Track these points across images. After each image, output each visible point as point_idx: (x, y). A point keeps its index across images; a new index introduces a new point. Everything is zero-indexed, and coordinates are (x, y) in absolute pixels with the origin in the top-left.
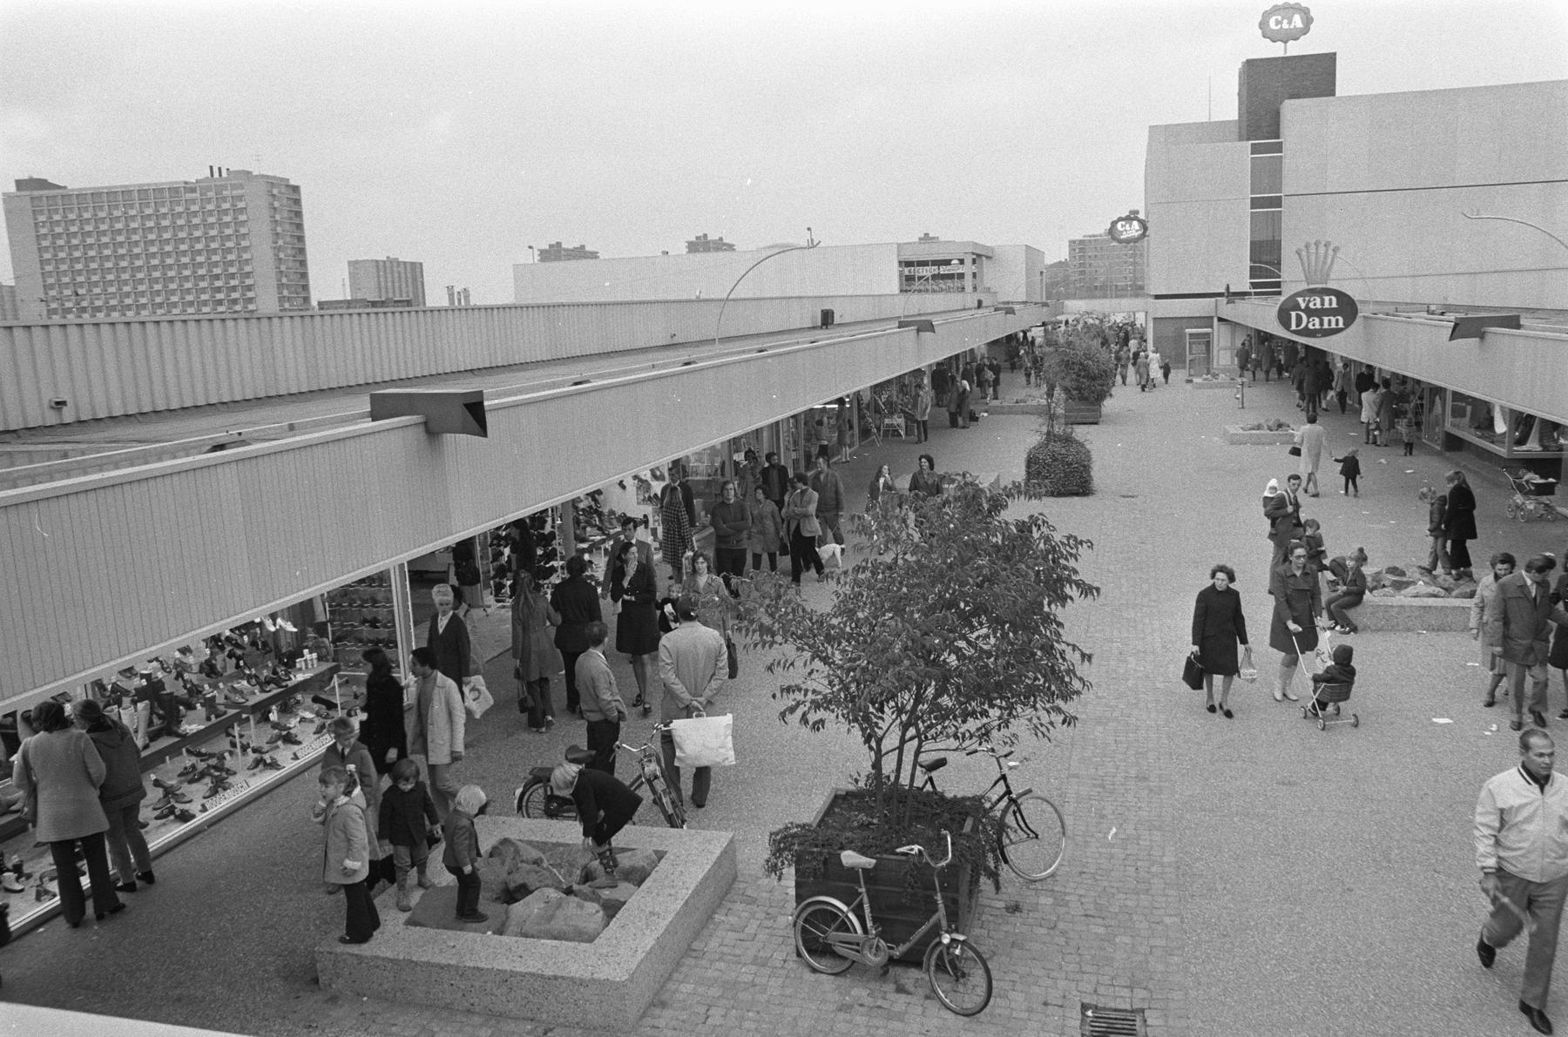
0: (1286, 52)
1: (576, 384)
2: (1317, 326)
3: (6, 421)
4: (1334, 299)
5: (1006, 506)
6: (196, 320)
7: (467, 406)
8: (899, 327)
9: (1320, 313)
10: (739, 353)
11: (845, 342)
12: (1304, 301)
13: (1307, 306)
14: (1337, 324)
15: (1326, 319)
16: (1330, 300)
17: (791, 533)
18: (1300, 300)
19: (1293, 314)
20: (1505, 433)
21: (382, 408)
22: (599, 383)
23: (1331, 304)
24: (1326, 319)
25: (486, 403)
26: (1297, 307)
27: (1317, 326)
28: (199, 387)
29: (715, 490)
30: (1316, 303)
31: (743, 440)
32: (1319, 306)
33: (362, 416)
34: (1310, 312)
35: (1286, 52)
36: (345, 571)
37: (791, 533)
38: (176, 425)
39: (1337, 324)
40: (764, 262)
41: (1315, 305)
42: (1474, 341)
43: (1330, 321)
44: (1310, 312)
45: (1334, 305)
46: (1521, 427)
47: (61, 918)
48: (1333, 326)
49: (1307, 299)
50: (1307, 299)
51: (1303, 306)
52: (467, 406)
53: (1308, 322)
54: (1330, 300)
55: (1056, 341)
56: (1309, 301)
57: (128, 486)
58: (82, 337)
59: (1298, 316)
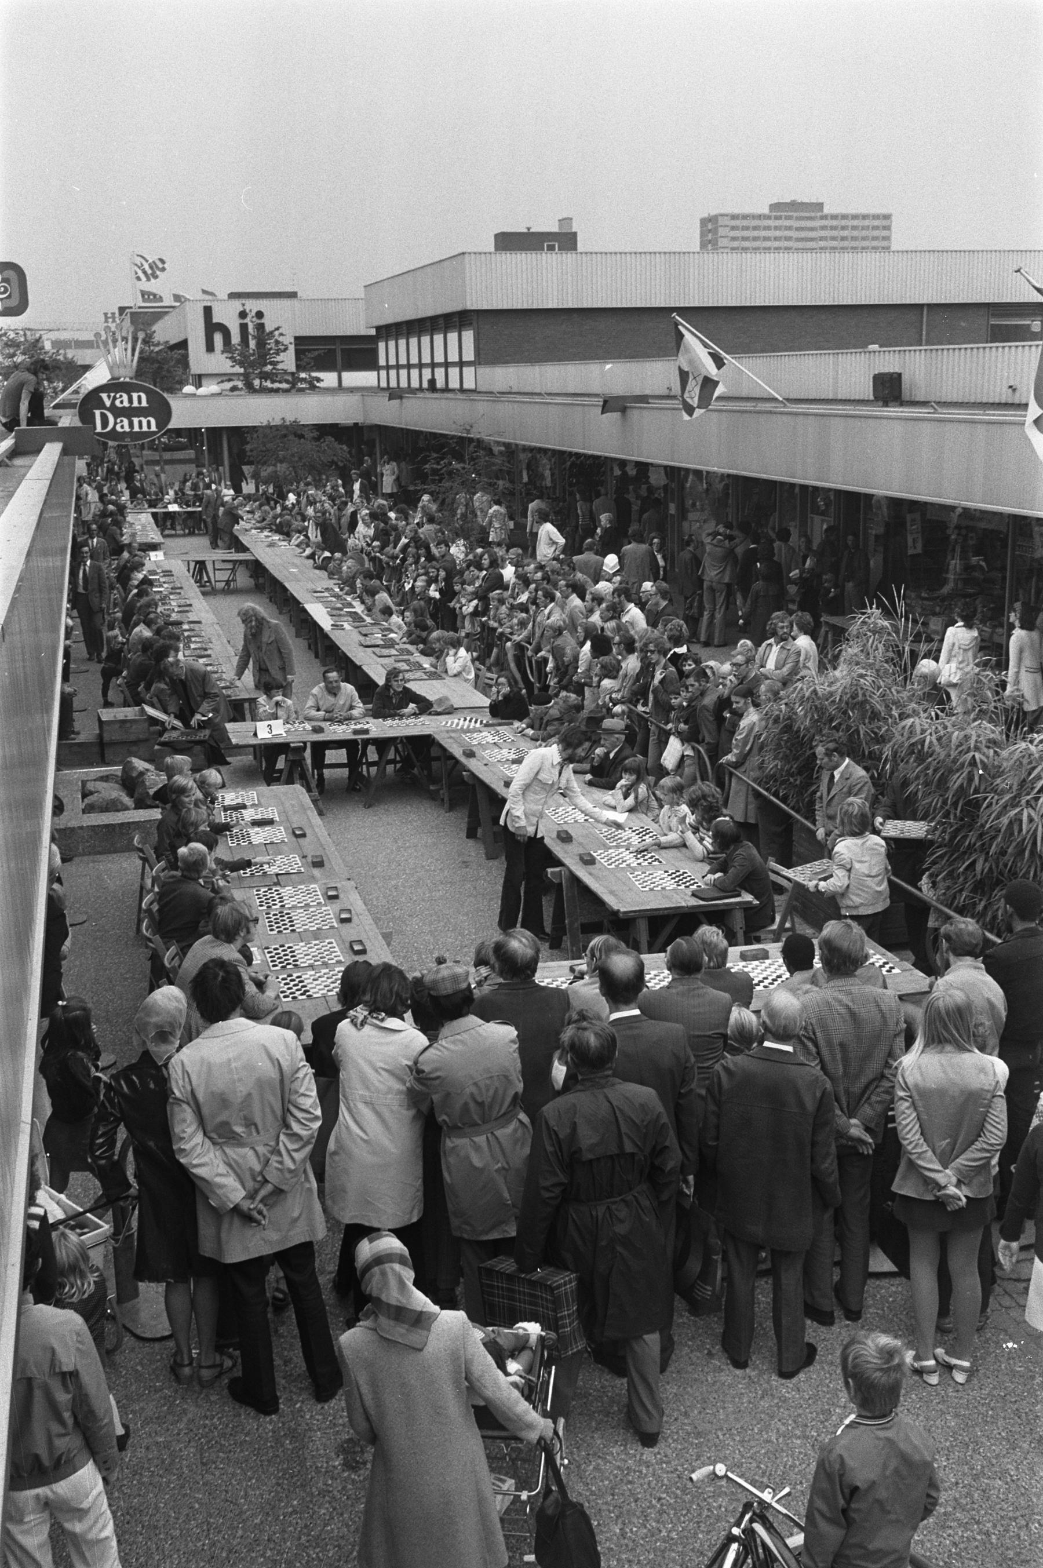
2: (127, 429)
4: (143, 396)
5: (330, 578)
9: (129, 413)
12: (109, 397)
13: (113, 403)
14: (149, 426)
15: (136, 420)
16: (139, 397)
18: (104, 396)
19: (97, 413)
20: (924, 657)
23: (140, 402)
24: (136, 420)
26: (101, 405)
27: (127, 429)
29: (993, 772)
30: (123, 401)
31: (275, 1273)
32: (126, 404)
34: (118, 412)
38: (878, 1283)
39: (149, 426)
41: (122, 402)
42: (398, 401)
43: (140, 422)
44: (118, 412)
45: (144, 404)
46: (471, 782)
47: (463, 333)
48: (145, 428)
49: (112, 395)
50: (112, 395)
51: (108, 403)
53: (116, 424)
54: (139, 397)
56: (115, 398)
59: (103, 416)
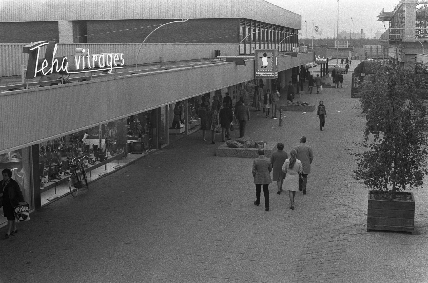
8: (226, 62)
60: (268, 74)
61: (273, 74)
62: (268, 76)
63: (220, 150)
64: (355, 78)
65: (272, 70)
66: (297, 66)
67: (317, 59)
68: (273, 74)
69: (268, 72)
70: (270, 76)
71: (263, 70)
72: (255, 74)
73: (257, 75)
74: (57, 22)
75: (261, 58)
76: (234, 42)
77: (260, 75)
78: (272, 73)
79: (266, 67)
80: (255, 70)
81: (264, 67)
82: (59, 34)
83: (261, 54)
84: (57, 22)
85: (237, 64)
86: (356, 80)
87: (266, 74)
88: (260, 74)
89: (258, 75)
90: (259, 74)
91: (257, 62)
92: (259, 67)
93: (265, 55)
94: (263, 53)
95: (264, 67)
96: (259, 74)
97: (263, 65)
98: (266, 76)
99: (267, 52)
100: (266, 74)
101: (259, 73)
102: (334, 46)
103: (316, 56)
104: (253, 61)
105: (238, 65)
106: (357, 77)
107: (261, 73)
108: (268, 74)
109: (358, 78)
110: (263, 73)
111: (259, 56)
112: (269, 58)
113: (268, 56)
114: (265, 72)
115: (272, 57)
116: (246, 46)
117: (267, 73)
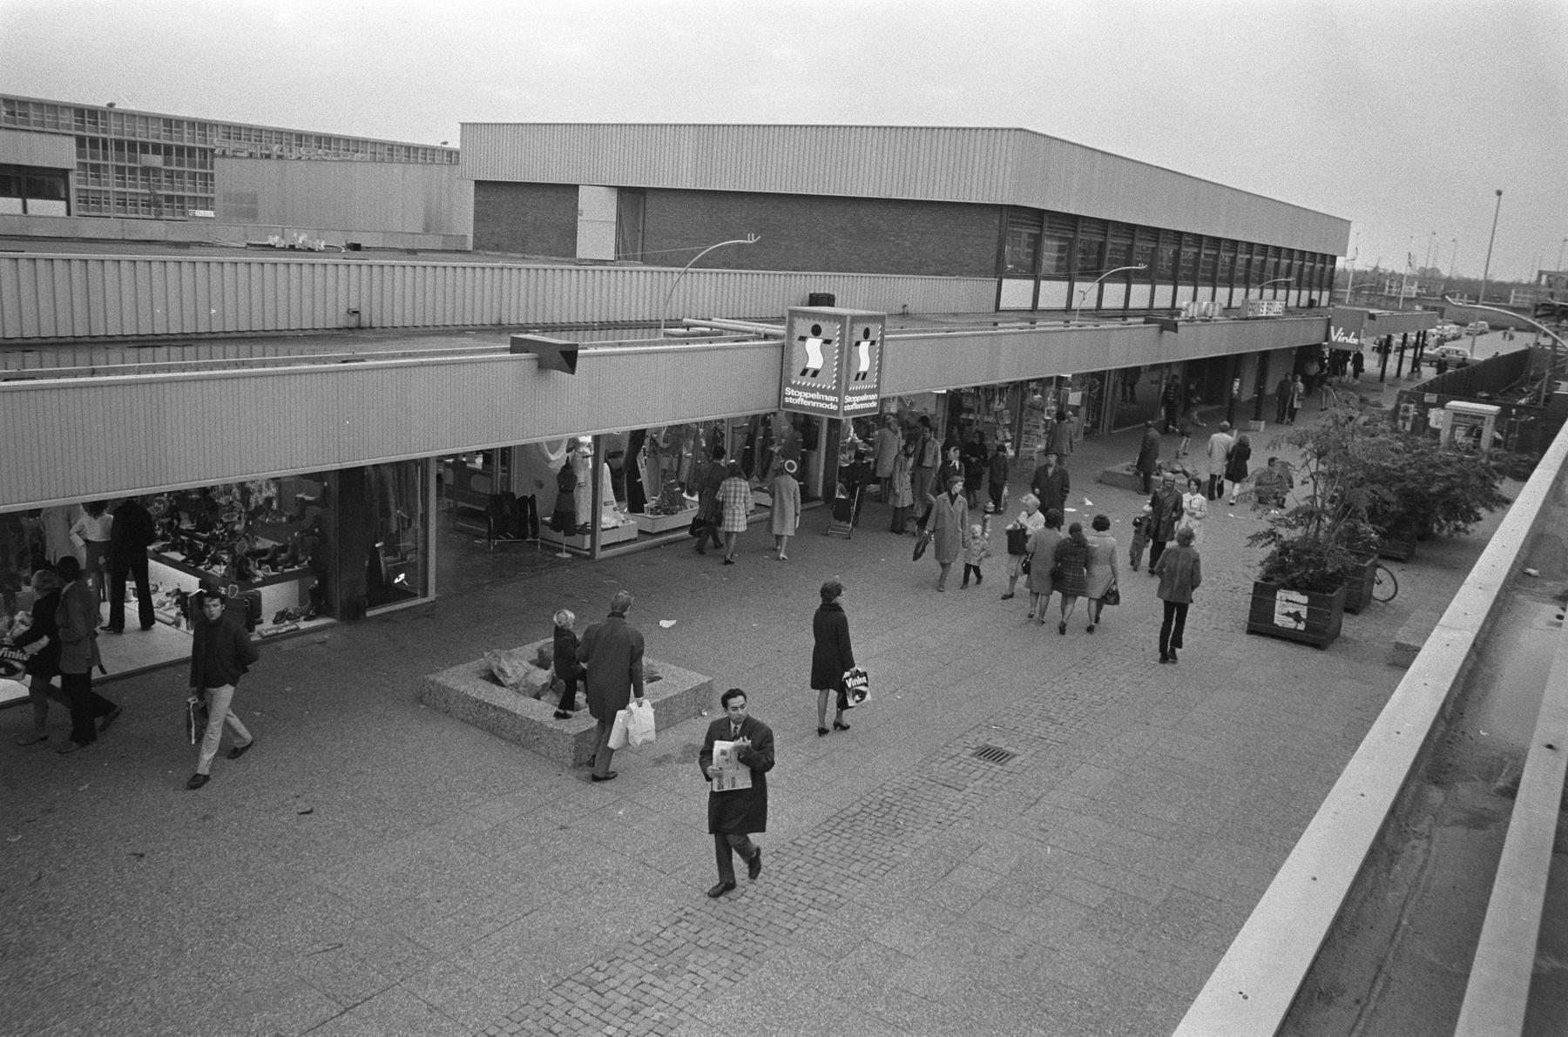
0: (733, 786)
1: (6, 380)
3: (4, 333)
6: (29, 259)
7: (562, 352)
8: (1145, 323)
10: (404, 356)
11: (939, 337)
17: (12, 662)
21: (517, 346)
22: (306, 367)
25: (580, 351)
28: (581, 313)
33: (505, 350)
35: (733, 786)
36: (23, 499)
37: (12, 662)
40: (1489, 239)
52: (562, 352)
55: (1286, 414)
57: (17, 394)
58: (528, 276)
60: (822, 401)
61: (834, 403)
62: (822, 405)
63: (433, 683)
64: (1403, 405)
65: (834, 388)
66: (1100, 369)
67: (1334, 338)
68: (834, 403)
69: (823, 391)
70: (827, 406)
71: (807, 381)
72: (781, 394)
73: (787, 400)
74: (576, 187)
75: (803, 339)
76: (984, 273)
77: (798, 401)
78: (832, 399)
79: (815, 373)
80: (783, 381)
81: (810, 373)
82: (579, 218)
83: (803, 327)
84: (576, 187)
85: (1162, 329)
86: (1407, 410)
87: (816, 400)
88: (797, 397)
89: (790, 400)
90: (794, 397)
91: (791, 352)
92: (797, 370)
93: (816, 331)
94: (812, 323)
95: (810, 373)
96: (794, 397)
97: (808, 366)
98: (814, 404)
99: (824, 321)
100: (816, 400)
101: (793, 392)
102: (1508, 302)
103: (1332, 328)
104: (780, 350)
105: (1166, 332)
106: (1412, 403)
107: (800, 394)
108: (822, 401)
109: (1412, 406)
110: (806, 395)
111: (798, 332)
112: (827, 342)
113: (825, 334)
114: (813, 390)
115: (838, 339)
116: (1105, 289)
117: (818, 396)
